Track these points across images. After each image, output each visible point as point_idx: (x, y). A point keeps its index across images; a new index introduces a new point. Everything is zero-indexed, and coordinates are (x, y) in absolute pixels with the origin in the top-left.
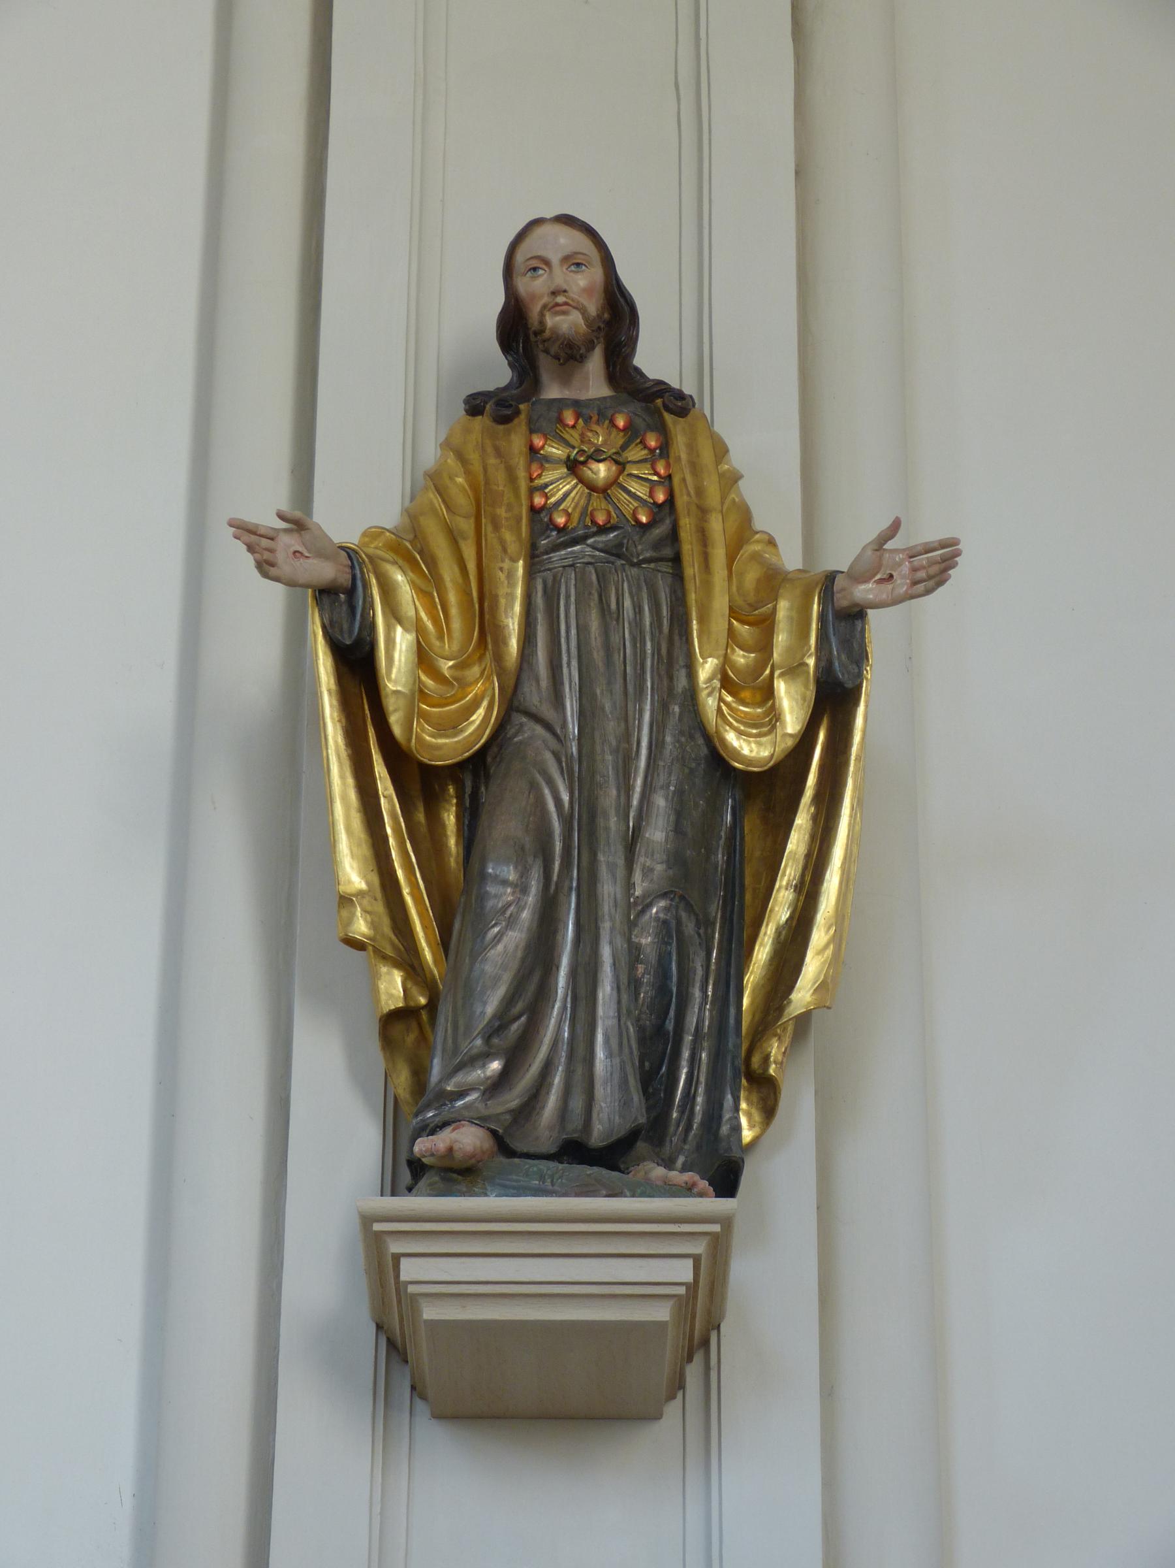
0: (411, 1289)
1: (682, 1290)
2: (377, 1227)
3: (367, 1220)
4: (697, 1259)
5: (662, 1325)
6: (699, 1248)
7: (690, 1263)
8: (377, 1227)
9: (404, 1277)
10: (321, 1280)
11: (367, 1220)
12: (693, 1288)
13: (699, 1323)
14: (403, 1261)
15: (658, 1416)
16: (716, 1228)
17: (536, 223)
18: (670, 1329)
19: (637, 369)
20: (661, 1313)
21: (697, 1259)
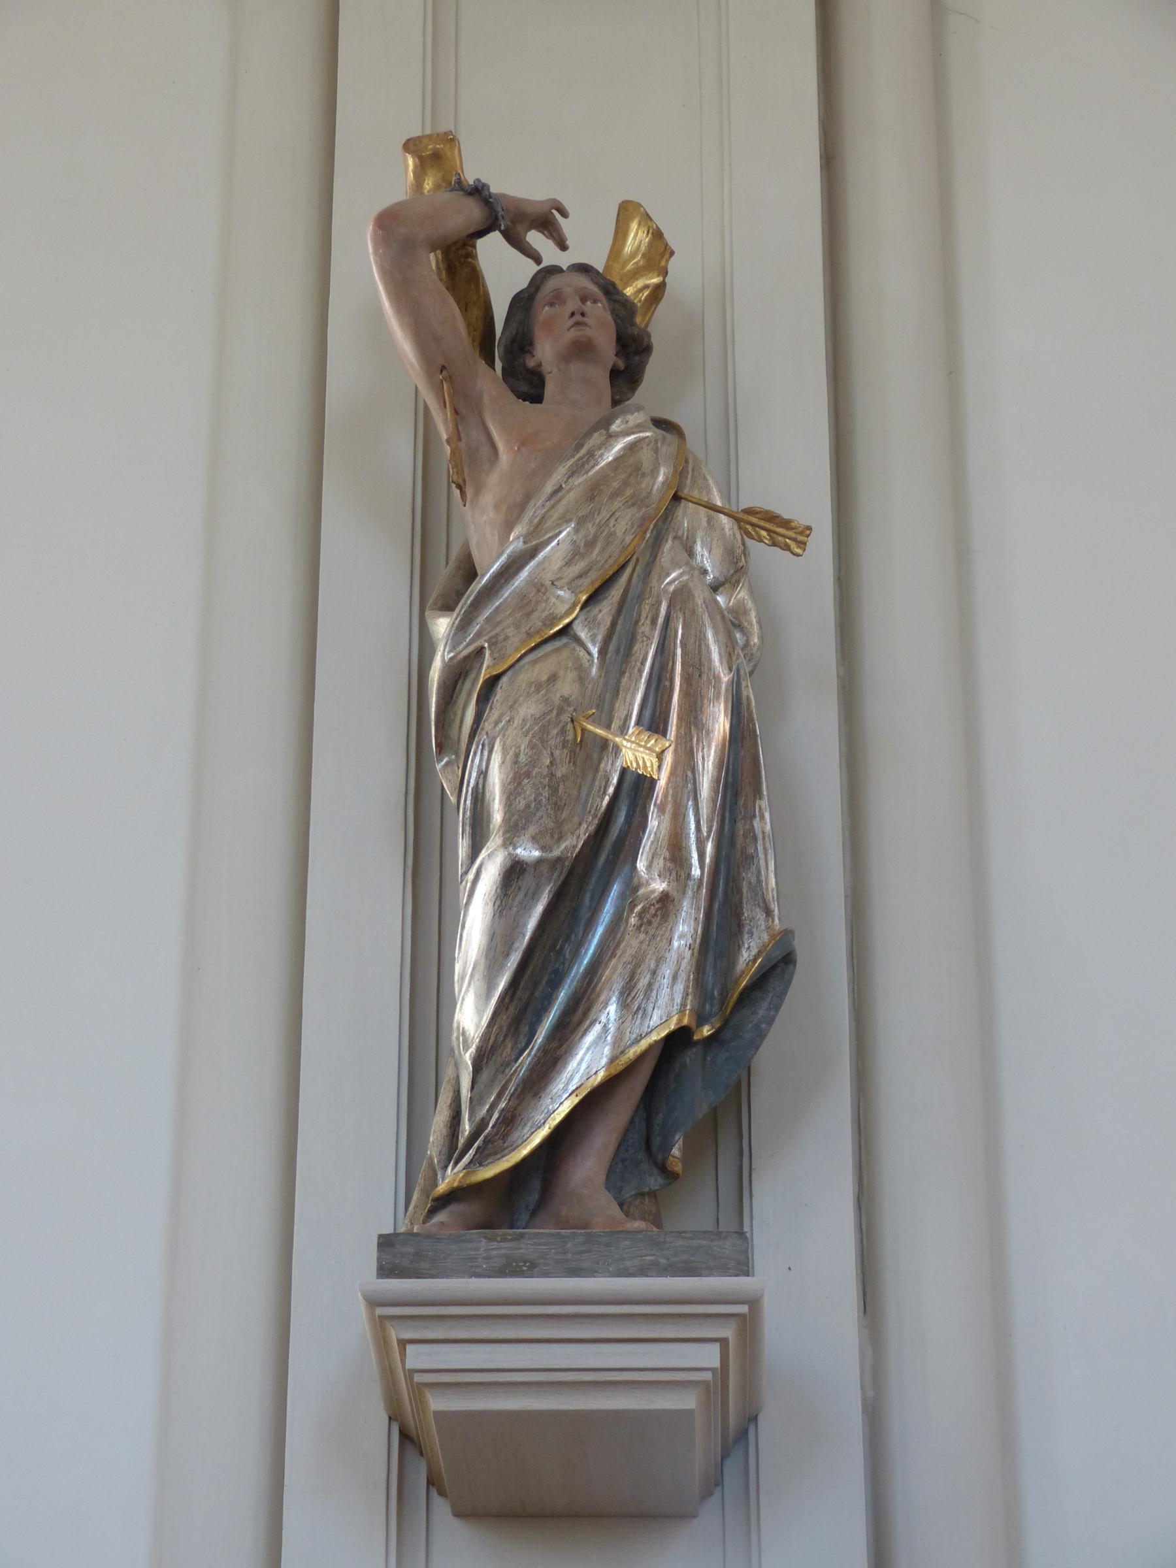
0: (418, 1378)
1: (708, 1376)
2: (380, 1311)
3: (373, 1302)
4: (723, 1342)
7: (716, 1347)
13: (737, 1436)
16: (743, 1309)
20: (688, 1402)
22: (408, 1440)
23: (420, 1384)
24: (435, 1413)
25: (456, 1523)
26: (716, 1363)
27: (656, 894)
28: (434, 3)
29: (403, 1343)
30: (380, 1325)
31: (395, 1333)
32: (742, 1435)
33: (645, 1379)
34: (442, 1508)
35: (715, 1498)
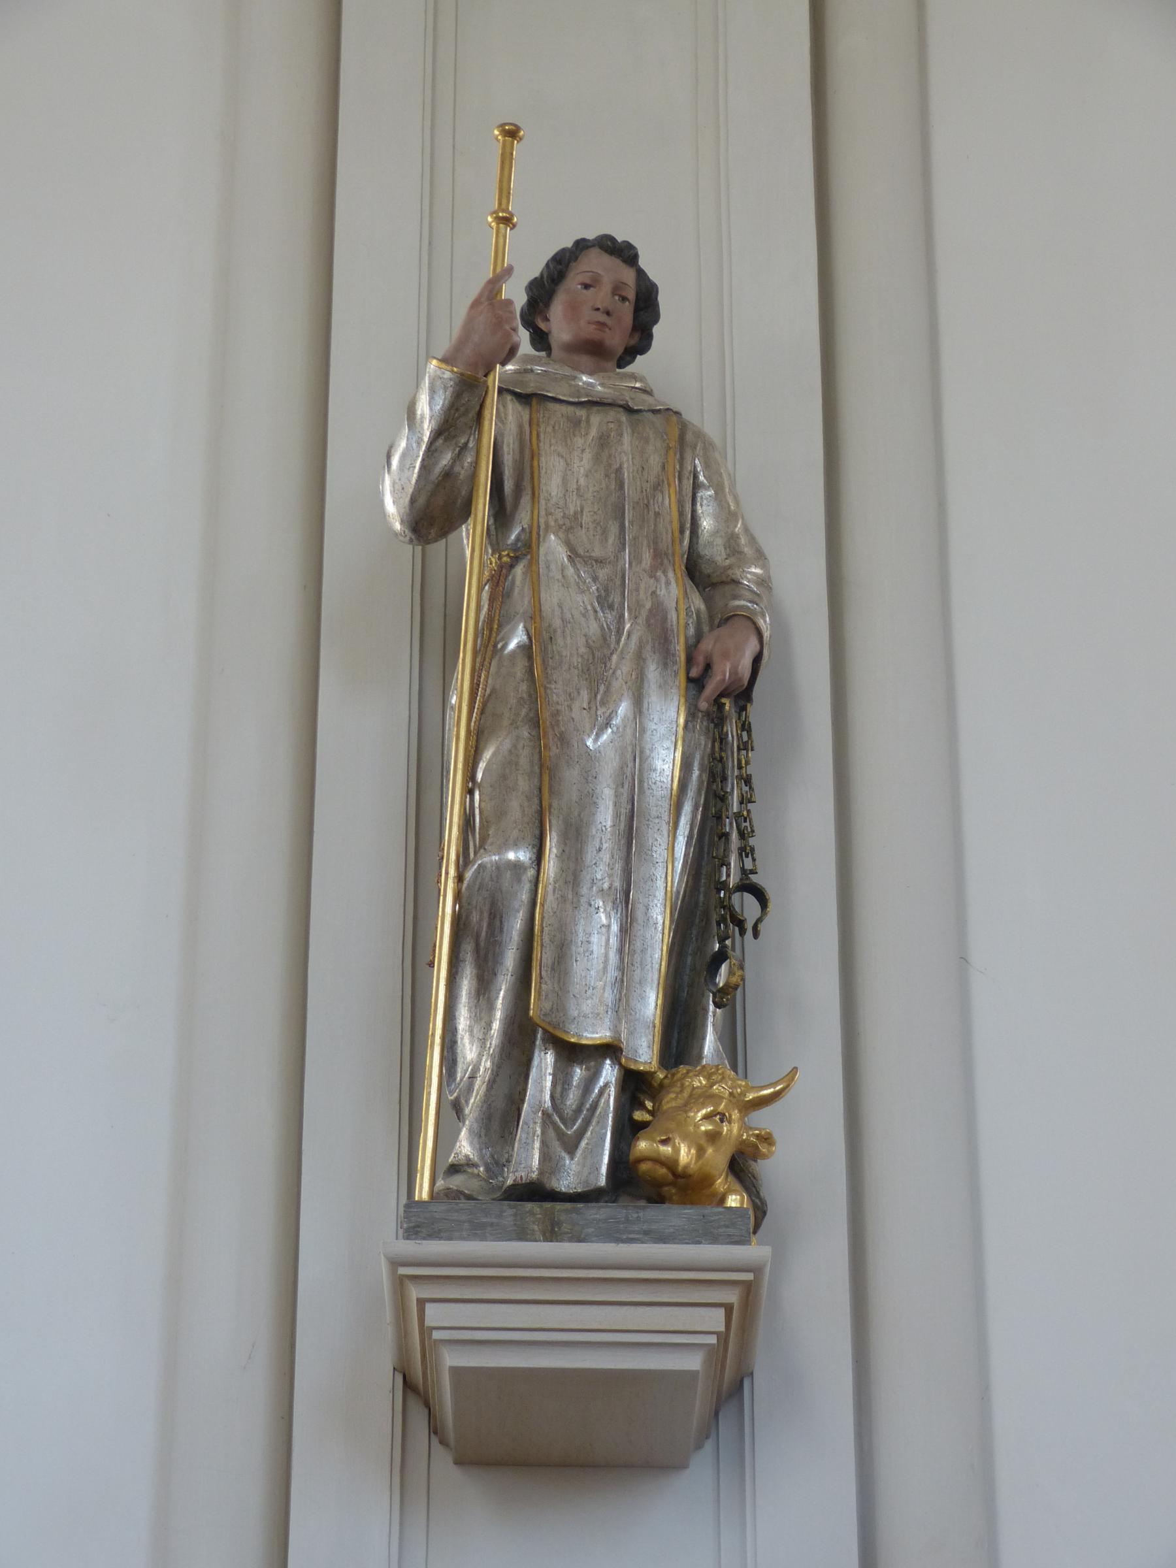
0: (436, 1335)
1: (713, 1340)
2: (403, 1271)
3: (395, 1263)
4: (729, 1308)
5: (693, 1375)
6: (732, 1297)
7: (721, 1312)
8: (403, 1271)
9: (429, 1322)
10: (341, 1346)
11: (395, 1263)
12: (724, 1338)
13: (730, 1386)
14: (428, 1306)
15: (683, 1466)
16: (749, 1276)
17: (582, 245)
18: (700, 1385)
19: (635, 358)
20: (693, 1362)
21: (729, 1308)
22: (413, 1388)
23: (436, 1341)
24: (456, 1372)
25: (456, 1473)
26: (722, 1328)
27: (578, 712)
28: (436, 3)
29: (421, 1303)
30: (400, 1284)
31: (415, 1292)
32: (737, 1389)
33: (591, 1276)
34: (443, 1459)
35: (709, 1445)
